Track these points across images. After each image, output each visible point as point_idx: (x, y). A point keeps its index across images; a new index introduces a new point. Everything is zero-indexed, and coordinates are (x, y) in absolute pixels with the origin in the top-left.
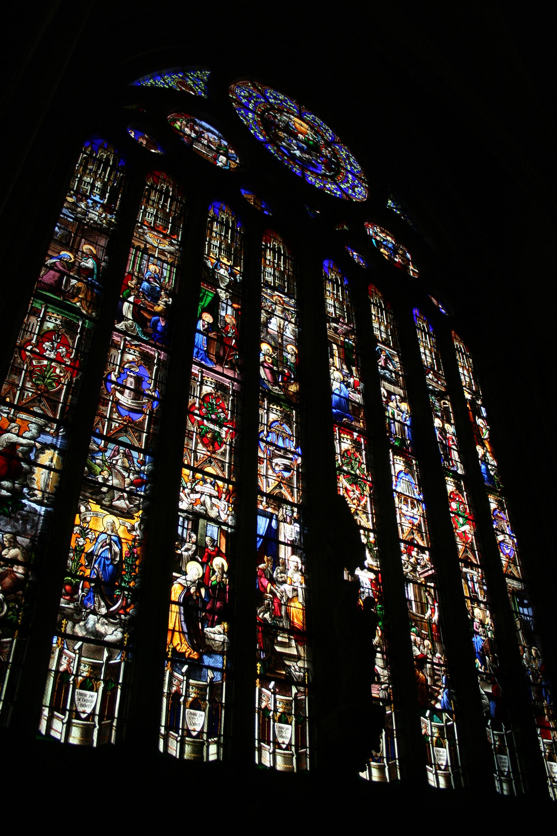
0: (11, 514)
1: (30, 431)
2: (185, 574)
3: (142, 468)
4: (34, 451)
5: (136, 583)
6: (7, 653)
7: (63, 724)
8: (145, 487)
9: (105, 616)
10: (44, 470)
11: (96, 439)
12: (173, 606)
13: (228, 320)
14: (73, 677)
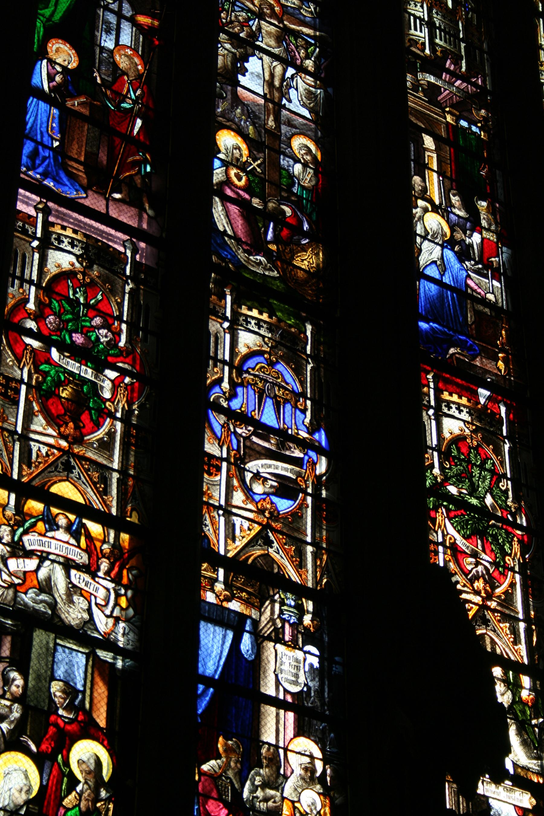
13: (122, 62)
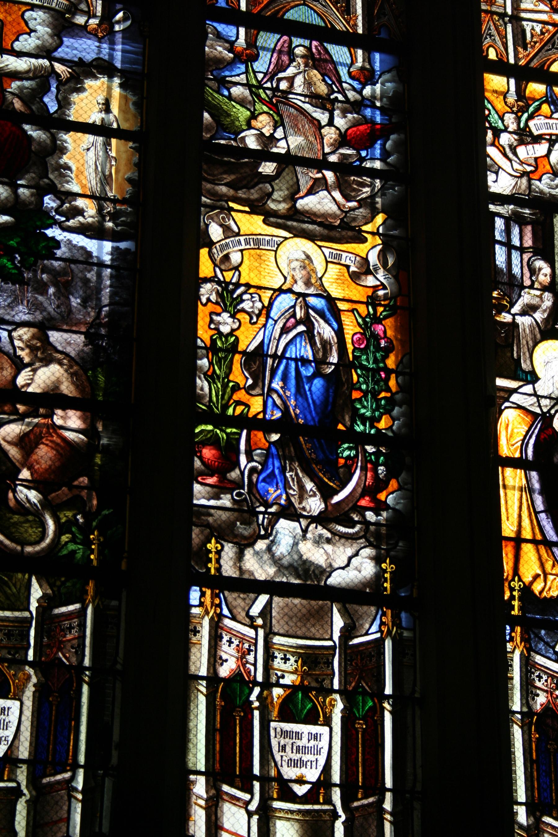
0: (21, 274)
1: (32, 31)
2: (532, 377)
3: (367, 91)
4: (53, 89)
5: (394, 420)
6: (75, 642)
7: (250, 814)
8: (383, 146)
9: (321, 519)
10: (90, 138)
11: (221, 27)
12: (509, 471)
14: (257, 690)
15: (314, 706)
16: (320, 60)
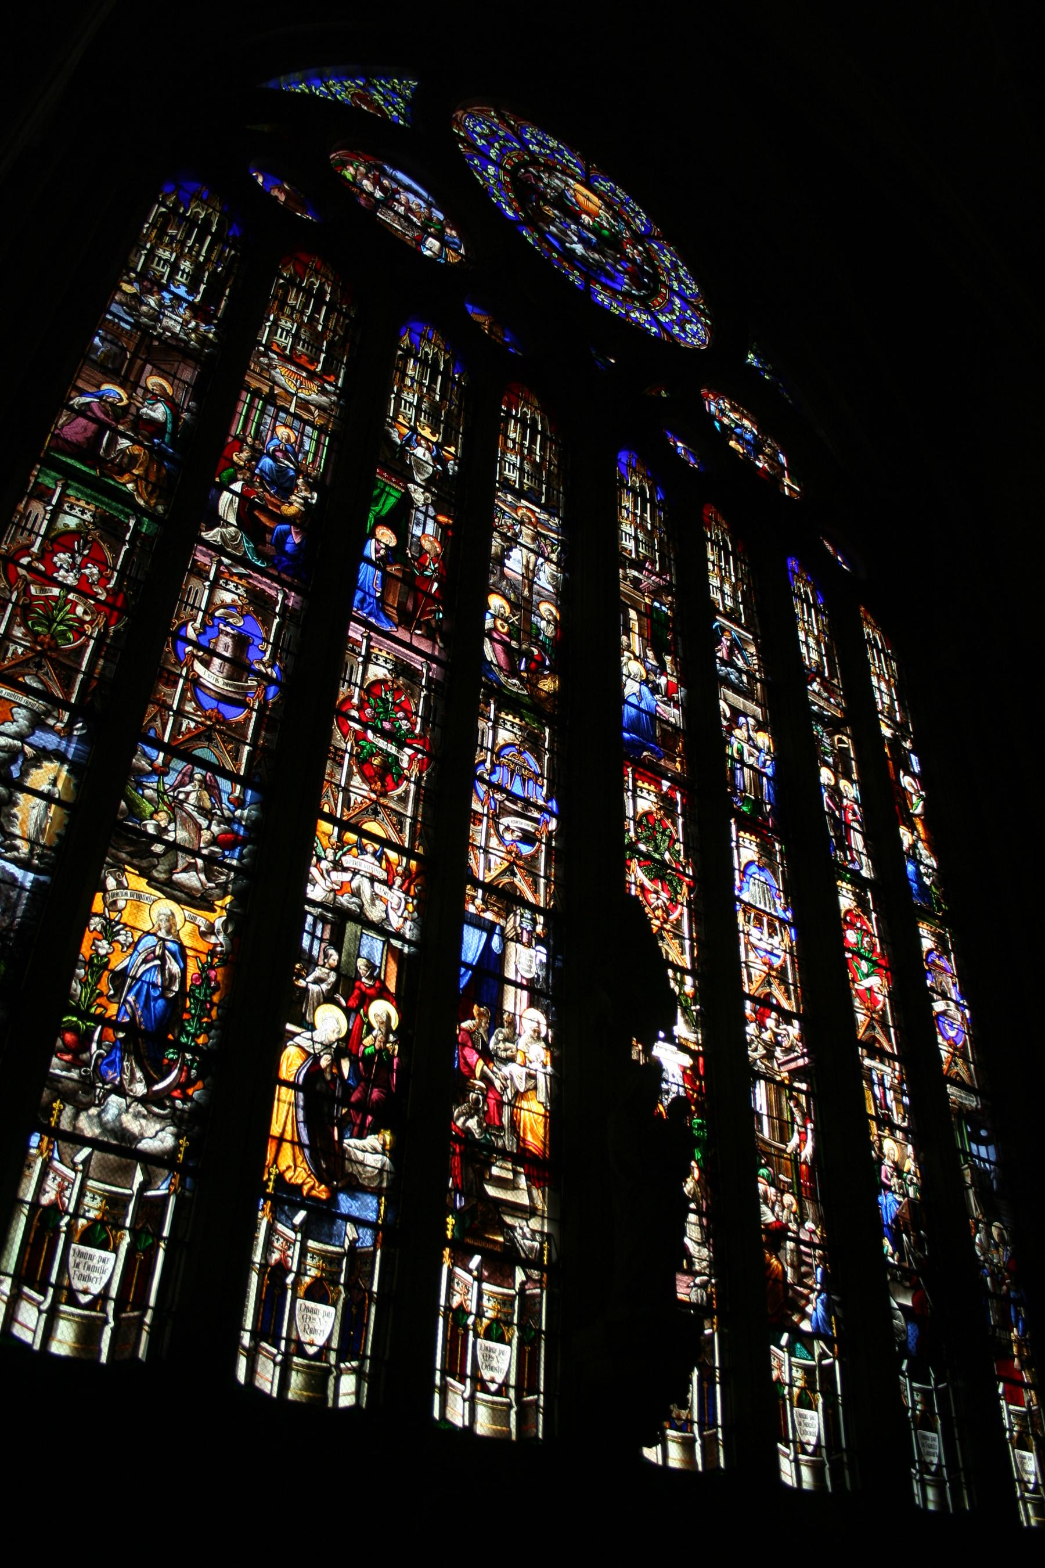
2: (311, 1027)
3: (238, 813)
4: (20, 762)
7: (40, 1312)
9: (143, 1100)
10: (38, 800)
11: (147, 749)
12: (284, 1089)
13: (427, 545)
14: (67, 1219)
15: (108, 1237)
16: (210, 786)
